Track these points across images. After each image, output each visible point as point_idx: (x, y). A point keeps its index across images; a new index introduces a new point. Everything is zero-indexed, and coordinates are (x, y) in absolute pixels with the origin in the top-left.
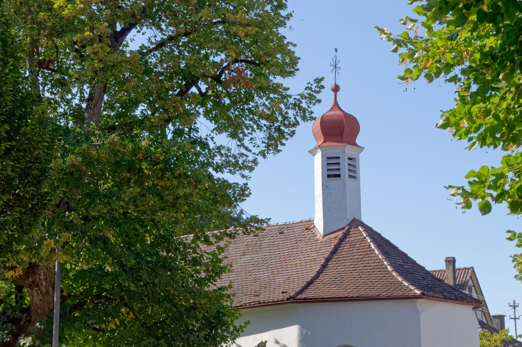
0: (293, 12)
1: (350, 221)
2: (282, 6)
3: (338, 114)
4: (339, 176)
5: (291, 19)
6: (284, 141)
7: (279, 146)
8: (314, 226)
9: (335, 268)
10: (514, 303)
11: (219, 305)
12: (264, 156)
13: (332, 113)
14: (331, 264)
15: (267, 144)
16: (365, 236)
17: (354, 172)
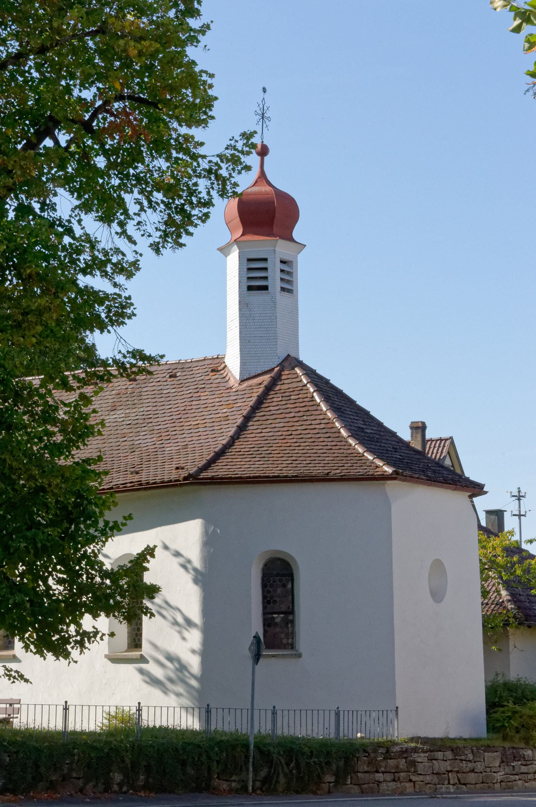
0: (212, 22)
1: (282, 358)
2: (194, 13)
3: (266, 191)
4: (265, 288)
5: (208, 33)
6: (191, 229)
7: (184, 235)
8: (226, 366)
9: (259, 431)
10: (519, 492)
11: (83, 487)
12: (157, 251)
13: (256, 189)
14: (252, 425)
15: (165, 231)
16: (305, 382)
17: (289, 282)
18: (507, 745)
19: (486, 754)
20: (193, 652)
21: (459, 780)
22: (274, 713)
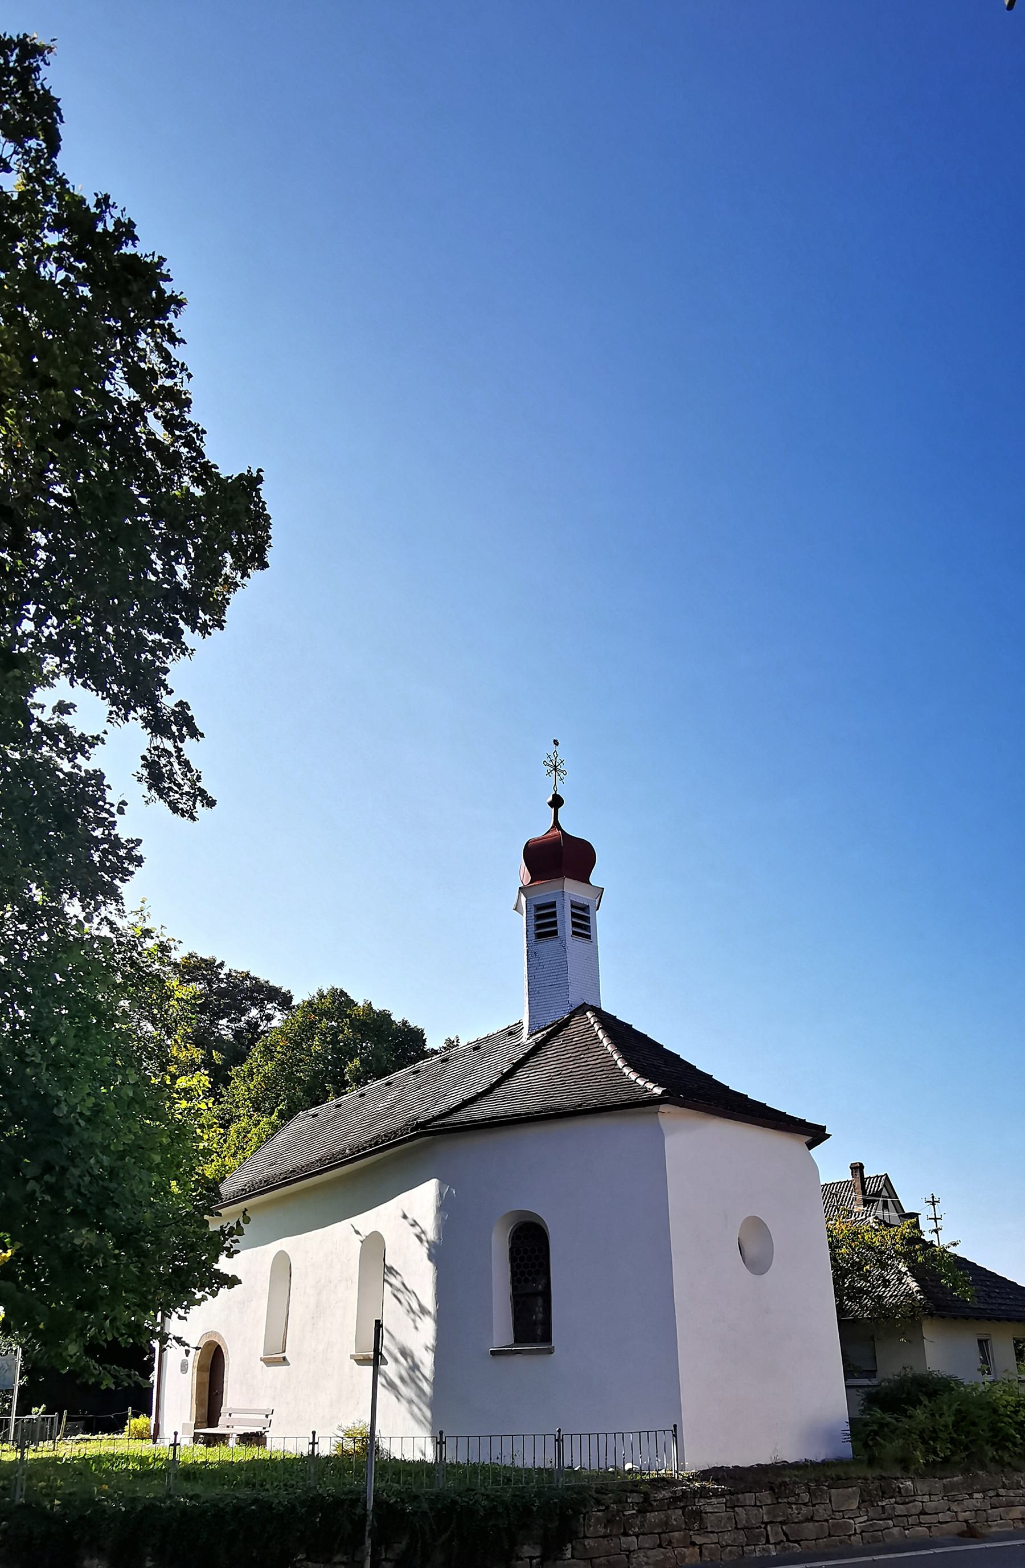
18: (870, 1474)
19: (833, 1491)
20: (427, 1348)
21: (785, 1534)
22: (559, 1440)
